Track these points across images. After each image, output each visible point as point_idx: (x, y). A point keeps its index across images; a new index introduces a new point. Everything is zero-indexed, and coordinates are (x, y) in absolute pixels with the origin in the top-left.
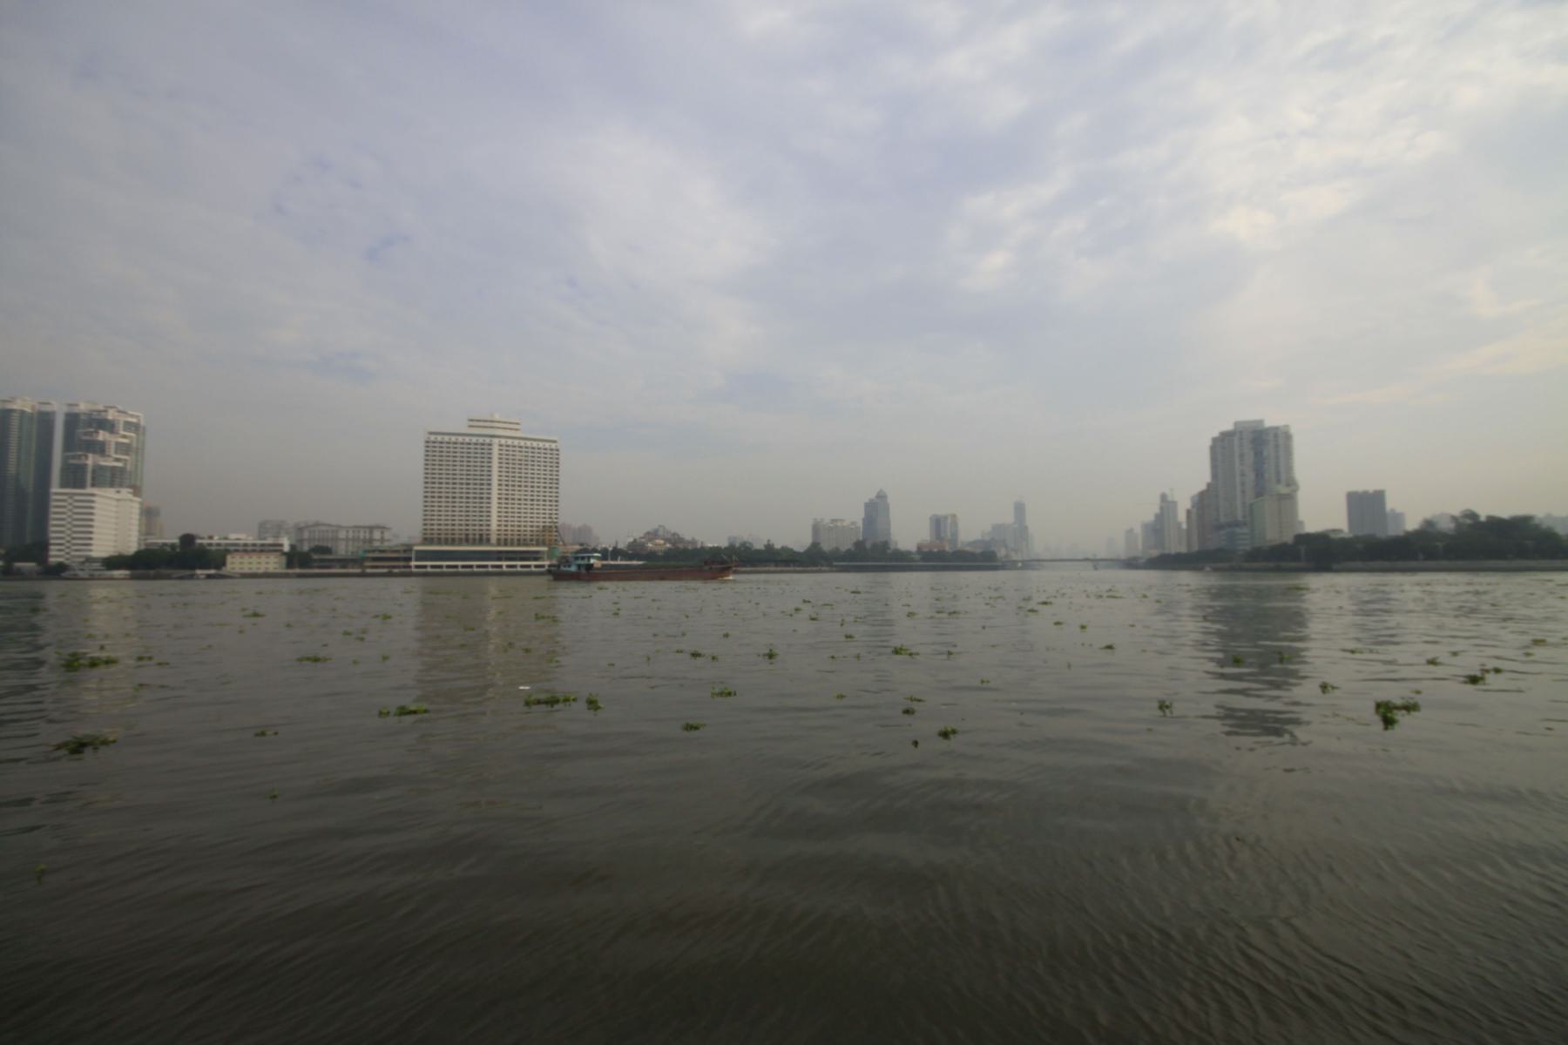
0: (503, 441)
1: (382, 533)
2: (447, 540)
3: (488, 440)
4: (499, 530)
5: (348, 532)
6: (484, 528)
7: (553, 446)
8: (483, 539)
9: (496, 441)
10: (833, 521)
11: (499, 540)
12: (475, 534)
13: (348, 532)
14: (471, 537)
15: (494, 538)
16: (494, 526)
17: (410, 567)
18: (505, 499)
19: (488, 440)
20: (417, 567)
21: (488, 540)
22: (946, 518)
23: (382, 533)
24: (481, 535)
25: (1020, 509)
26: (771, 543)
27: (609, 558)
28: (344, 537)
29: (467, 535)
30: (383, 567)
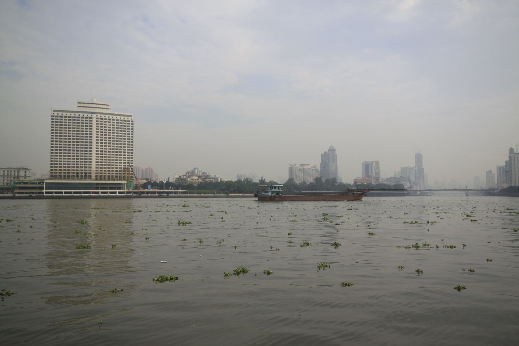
0: (99, 116)
1: (25, 172)
2: (69, 176)
3: (90, 115)
4: (96, 171)
5: (4, 171)
6: (88, 169)
7: (130, 119)
8: (87, 176)
9: (95, 116)
10: (302, 165)
11: (96, 176)
12: (82, 173)
13: (4, 171)
14: (80, 174)
15: (93, 176)
16: (94, 168)
17: (43, 193)
18: (100, 152)
19: (90, 115)
20: (46, 193)
21: (90, 176)
22: (372, 163)
23: (25, 172)
24: (86, 173)
25: (419, 158)
26: (263, 179)
27: (117, 189)
28: (2, 175)
29: (77, 173)
30: (26, 193)
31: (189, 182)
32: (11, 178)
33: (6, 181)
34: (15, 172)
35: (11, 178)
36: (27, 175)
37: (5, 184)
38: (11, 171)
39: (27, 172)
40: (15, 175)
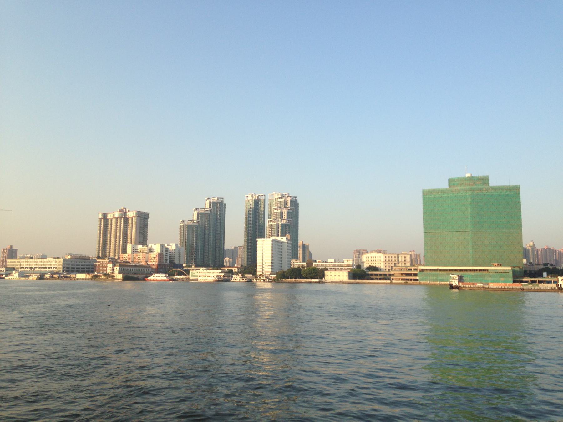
1: (405, 257)
31: (362, 251)
32: (392, 264)
33: (388, 267)
34: (395, 257)
35: (392, 264)
36: (406, 261)
37: (387, 270)
38: (392, 257)
40: (395, 260)
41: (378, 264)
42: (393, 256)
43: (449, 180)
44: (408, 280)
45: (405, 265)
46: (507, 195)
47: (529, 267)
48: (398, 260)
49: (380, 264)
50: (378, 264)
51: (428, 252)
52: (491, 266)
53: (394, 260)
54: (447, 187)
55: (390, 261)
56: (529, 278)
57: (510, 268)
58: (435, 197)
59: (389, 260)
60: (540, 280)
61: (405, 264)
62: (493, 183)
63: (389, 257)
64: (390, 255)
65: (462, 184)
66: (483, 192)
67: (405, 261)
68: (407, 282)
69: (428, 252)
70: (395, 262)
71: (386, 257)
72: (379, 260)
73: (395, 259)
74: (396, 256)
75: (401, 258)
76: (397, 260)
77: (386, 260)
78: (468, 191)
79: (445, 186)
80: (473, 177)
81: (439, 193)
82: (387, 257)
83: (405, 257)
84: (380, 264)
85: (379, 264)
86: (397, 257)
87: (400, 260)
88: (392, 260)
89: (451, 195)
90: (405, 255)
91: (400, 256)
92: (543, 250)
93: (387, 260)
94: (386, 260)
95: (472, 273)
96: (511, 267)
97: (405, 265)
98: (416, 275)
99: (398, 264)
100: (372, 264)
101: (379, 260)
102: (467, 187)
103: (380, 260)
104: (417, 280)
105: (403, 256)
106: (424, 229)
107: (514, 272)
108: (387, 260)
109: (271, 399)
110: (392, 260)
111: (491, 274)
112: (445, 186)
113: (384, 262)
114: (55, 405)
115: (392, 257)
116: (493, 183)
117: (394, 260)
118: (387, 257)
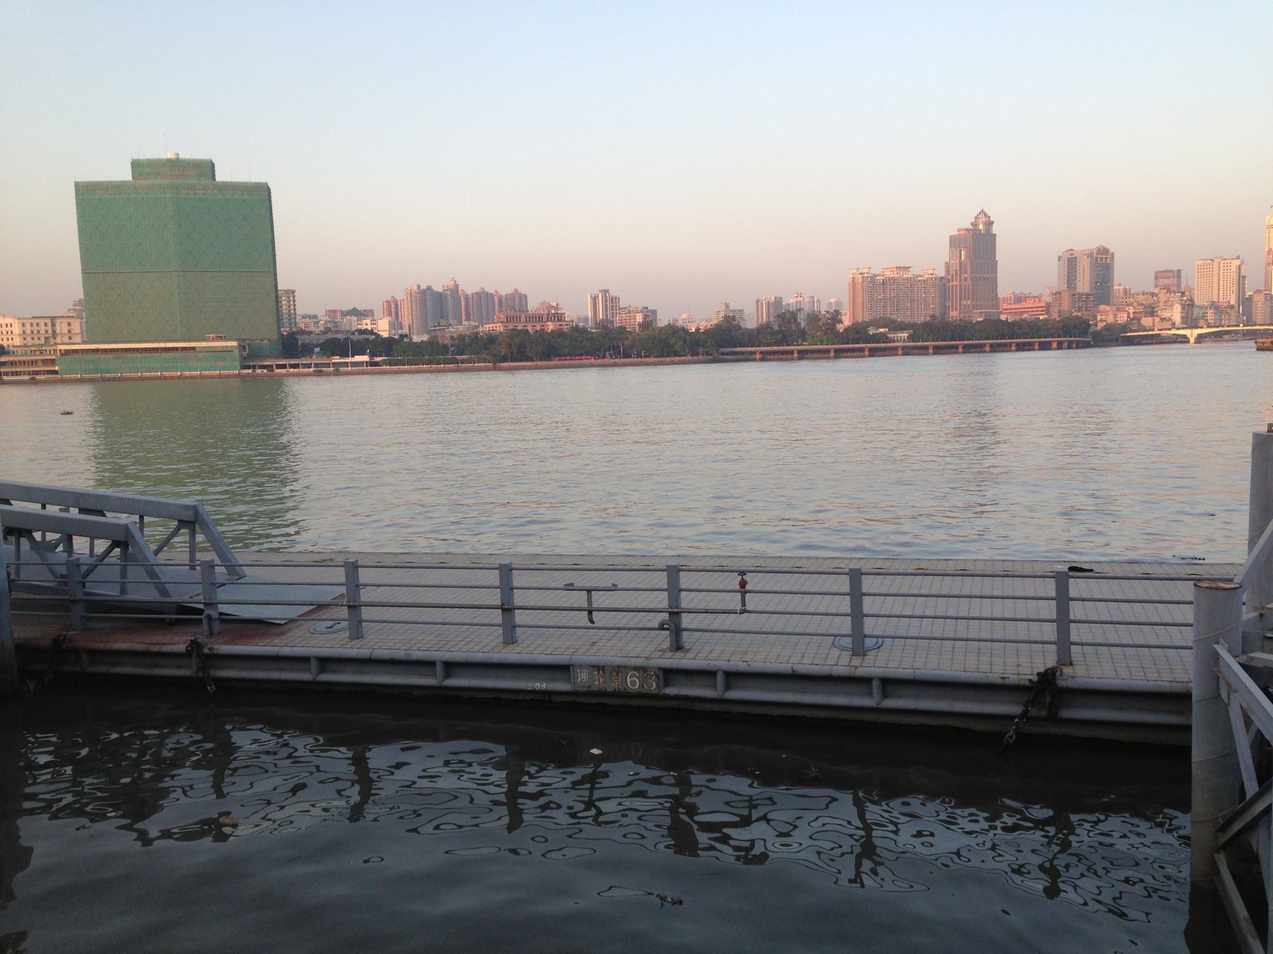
1: (69, 324)
25: (727, 306)
34: (46, 325)
35: (39, 339)
36: (73, 332)
38: (38, 325)
39: (72, 324)
40: (47, 332)
41: (8, 339)
42: (42, 322)
43: (132, 163)
44: (38, 373)
45: (71, 341)
46: (244, 201)
47: (317, 337)
48: (54, 332)
49: (12, 339)
50: (8, 339)
51: (92, 314)
52: (204, 340)
53: (43, 331)
54: (131, 179)
55: (36, 332)
56: (274, 360)
57: (235, 343)
58: (101, 199)
59: (32, 332)
60: (291, 363)
61: (70, 338)
62: (222, 176)
63: (32, 325)
64: (35, 321)
65: (159, 174)
66: (197, 192)
67: (69, 331)
68: (34, 379)
69: (92, 314)
70: (47, 336)
71: (23, 325)
72: (10, 333)
73: (32, 328)
74: (49, 321)
75: (61, 327)
76: (50, 331)
77: (24, 332)
78: (166, 190)
79: (126, 175)
80: (178, 159)
81: (110, 191)
82: (28, 325)
83: (69, 324)
84: (12, 339)
85: (10, 339)
86: (49, 325)
87: (58, 331)
88: (38, 332)
89: (134, 196)
90: (70, 320)
91: (58, 322)
92: (508, 296)
93: (28, 332)
94: (24, 332)
95: (166, 355)
96: (236, 340)
97: (71, 341)
98: (53, 362)
99: (55, 338)
100: (36, 339)
101: (10, 333)
102: (165, 182)
103: (12, 332)
104: (55, 372)
105: (65, 321)
106: (82, 266)
107: (242, 348)
108: (28, 332)
109: (471, 531)
110: (38, 332)
111: (201, 355)
112: (126, 175)
113: (20, 335)
114: (719, 490)
115: (38, 325)
116: (222, 176)
117: (43, 331)
118: (28, 325)
